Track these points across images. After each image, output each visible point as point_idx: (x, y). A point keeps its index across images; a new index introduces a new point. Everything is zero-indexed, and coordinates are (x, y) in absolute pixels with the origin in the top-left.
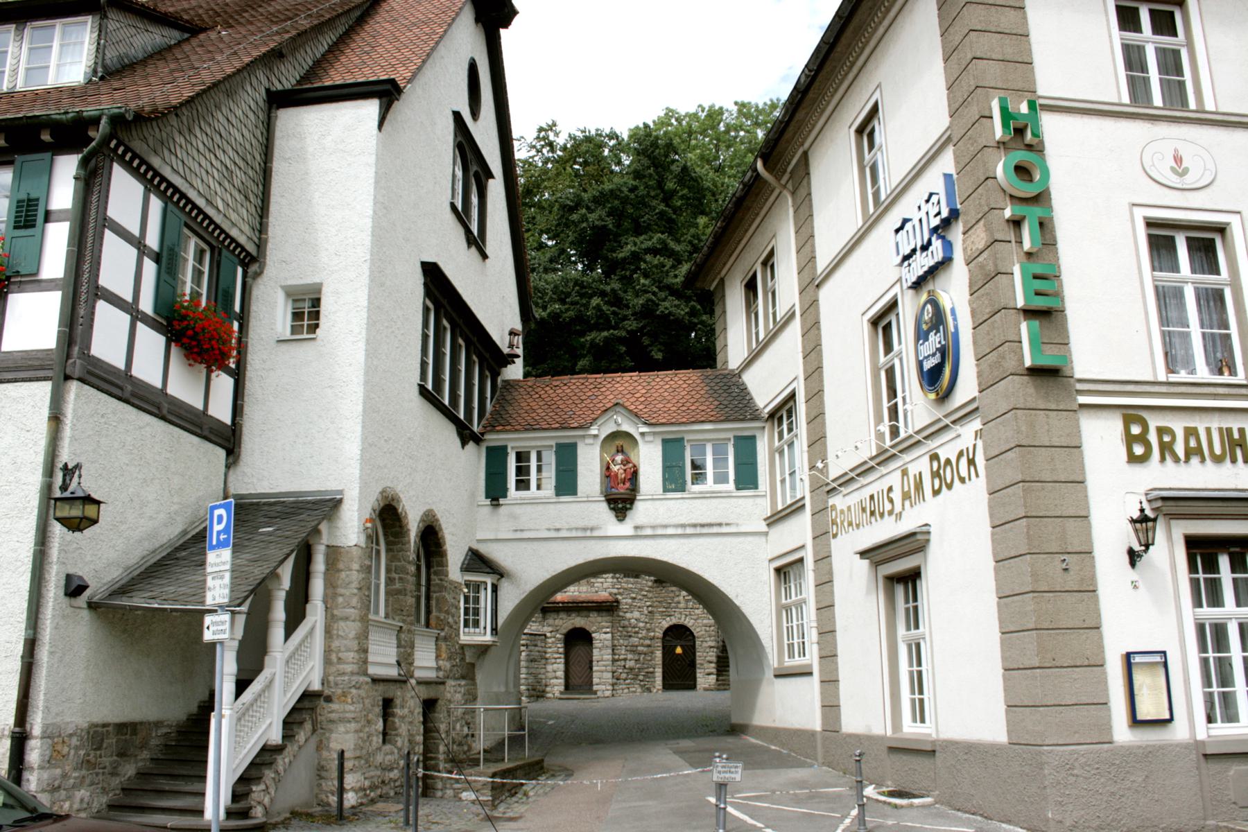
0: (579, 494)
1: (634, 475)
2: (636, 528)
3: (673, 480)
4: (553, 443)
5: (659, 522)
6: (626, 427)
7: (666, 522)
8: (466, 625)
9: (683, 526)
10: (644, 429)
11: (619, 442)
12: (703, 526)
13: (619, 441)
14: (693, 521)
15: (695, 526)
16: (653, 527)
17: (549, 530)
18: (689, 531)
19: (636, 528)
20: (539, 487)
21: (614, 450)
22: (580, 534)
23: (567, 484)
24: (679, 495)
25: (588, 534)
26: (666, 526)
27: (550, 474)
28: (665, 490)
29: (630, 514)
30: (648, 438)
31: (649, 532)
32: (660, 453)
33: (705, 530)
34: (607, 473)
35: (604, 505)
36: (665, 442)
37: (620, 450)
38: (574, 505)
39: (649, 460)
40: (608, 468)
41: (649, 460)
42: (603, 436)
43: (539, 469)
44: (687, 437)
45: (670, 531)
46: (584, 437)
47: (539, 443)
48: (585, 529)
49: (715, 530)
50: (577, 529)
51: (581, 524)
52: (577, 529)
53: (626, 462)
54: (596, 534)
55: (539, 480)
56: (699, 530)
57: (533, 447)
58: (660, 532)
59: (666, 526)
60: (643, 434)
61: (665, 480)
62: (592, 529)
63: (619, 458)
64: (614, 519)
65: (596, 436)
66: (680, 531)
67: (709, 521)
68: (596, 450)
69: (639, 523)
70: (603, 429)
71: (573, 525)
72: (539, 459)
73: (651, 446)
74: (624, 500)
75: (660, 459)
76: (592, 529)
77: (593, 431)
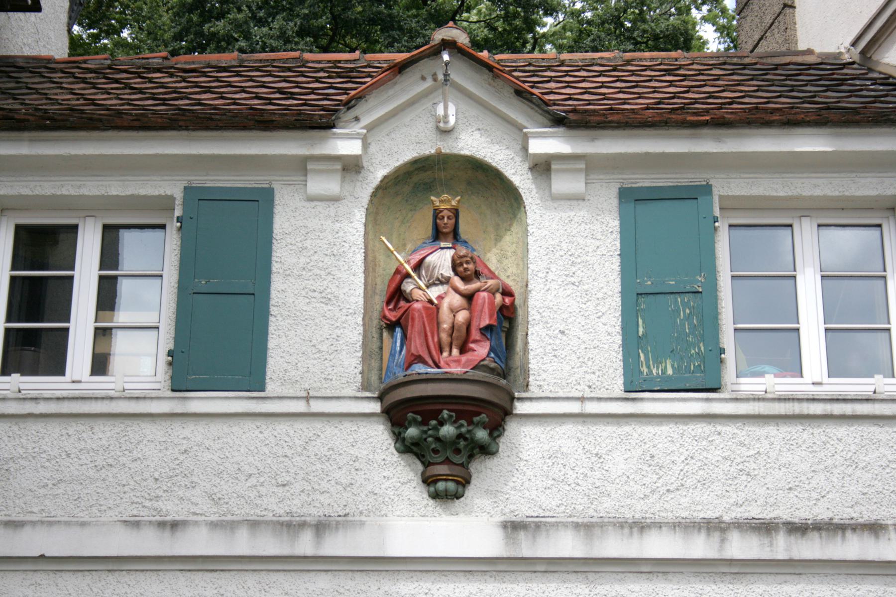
0: (272, 388)
1: (505, 322)
2: (513, 528)
3: (673, 342)
4: (172, 188)
5: (607, 507)
6: (474, 142)
7: (637, 510)
8: (427, 43)
9: (715, 527)
10: (549, 143)
11: (444, 201)
12: (798, 529)
13: (447, 194)
14: (755, 512)
15: (765, 528)
16: (587, 528)
17: (135, 524)
18: (741, 547)
19: (513, 528)
20: (100, 365)
21: (423, 226)
22: (269, 545)
23: (221, 345)
24: (693, 404)
25: (305, 545)
26: (641, 527)
27: (151, 305)
28: (635, 385)
29: (484, 472)
30: (562, 184)
31: (566, 545)
32: (613, 243)
33: (810, 548)
34: (394, 308)
35: (379, 435)
36: (632, 199)
37: (444, 231)
38: (249, 431)
39: (567, 266)
40: (397, 295)
41: (567, 266)
42: (378, 173)
43: (107, 297)
44: (726, 187)
45: (659, 546)
46: (301, 167)
47: (116, 188)
48: (291, 527)
49: (853, 548)
50: (254, 525)
51: (274, 506)
52: (254, 525)
53: (467, 269)
54: (336, 545)
55: (102, 334)
56: (782, 547)
57: (90, 206)
58: (614, 546)
59: (641, 527)
60: (542, 167)
61: (632, 344)
62: (321, 527)
63: (441, 260)
64: (417, 493)
65: (351, 167)
66: (700, 547)
67: (822, 513)
68: (354, 224)
69: (524, 511)
70: (388, 134)
71: (242, 511)
72: (110, 256)
73: (580, 213)
74: (466, 409)
75: (615, 264)
76: (321, 527)
77: (344, 144)
